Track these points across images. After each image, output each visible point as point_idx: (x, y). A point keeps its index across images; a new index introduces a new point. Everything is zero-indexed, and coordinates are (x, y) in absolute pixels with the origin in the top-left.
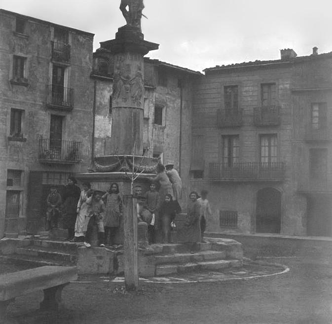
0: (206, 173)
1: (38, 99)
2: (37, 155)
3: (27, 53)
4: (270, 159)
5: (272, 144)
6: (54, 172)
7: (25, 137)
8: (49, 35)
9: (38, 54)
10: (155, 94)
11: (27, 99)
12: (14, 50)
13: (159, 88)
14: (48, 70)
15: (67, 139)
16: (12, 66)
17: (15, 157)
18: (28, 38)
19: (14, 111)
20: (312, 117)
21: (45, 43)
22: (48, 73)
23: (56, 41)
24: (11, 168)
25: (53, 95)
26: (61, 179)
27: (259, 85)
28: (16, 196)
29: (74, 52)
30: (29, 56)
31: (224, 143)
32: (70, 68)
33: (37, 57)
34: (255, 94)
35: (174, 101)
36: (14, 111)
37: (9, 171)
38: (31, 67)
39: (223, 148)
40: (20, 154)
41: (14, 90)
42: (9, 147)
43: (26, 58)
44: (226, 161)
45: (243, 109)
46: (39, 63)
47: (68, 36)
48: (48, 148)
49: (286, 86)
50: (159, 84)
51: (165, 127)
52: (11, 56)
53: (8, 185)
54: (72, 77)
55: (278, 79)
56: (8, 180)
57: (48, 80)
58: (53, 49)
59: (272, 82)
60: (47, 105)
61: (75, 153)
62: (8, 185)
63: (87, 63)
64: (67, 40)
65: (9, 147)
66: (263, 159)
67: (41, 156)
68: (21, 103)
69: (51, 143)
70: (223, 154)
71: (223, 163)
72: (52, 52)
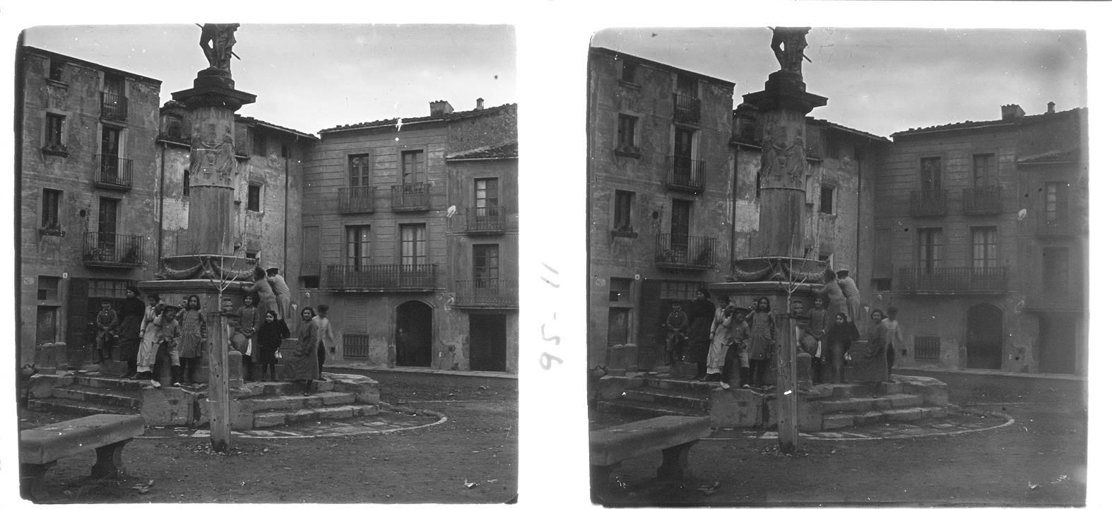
6: (105, 280)
8: (97, 84)
12: (47, 106)
16: (43, 127)
19: (47, 192)
20: (476, 199)
28: (51, 313)
31: (348, 237)
34: (393, 166)
35: (276, 178)
36: (47, 192)
39: (348, 243)
46: (83, 123)
50: (255, 153)
55: (427, 145)
56: (40, 291)
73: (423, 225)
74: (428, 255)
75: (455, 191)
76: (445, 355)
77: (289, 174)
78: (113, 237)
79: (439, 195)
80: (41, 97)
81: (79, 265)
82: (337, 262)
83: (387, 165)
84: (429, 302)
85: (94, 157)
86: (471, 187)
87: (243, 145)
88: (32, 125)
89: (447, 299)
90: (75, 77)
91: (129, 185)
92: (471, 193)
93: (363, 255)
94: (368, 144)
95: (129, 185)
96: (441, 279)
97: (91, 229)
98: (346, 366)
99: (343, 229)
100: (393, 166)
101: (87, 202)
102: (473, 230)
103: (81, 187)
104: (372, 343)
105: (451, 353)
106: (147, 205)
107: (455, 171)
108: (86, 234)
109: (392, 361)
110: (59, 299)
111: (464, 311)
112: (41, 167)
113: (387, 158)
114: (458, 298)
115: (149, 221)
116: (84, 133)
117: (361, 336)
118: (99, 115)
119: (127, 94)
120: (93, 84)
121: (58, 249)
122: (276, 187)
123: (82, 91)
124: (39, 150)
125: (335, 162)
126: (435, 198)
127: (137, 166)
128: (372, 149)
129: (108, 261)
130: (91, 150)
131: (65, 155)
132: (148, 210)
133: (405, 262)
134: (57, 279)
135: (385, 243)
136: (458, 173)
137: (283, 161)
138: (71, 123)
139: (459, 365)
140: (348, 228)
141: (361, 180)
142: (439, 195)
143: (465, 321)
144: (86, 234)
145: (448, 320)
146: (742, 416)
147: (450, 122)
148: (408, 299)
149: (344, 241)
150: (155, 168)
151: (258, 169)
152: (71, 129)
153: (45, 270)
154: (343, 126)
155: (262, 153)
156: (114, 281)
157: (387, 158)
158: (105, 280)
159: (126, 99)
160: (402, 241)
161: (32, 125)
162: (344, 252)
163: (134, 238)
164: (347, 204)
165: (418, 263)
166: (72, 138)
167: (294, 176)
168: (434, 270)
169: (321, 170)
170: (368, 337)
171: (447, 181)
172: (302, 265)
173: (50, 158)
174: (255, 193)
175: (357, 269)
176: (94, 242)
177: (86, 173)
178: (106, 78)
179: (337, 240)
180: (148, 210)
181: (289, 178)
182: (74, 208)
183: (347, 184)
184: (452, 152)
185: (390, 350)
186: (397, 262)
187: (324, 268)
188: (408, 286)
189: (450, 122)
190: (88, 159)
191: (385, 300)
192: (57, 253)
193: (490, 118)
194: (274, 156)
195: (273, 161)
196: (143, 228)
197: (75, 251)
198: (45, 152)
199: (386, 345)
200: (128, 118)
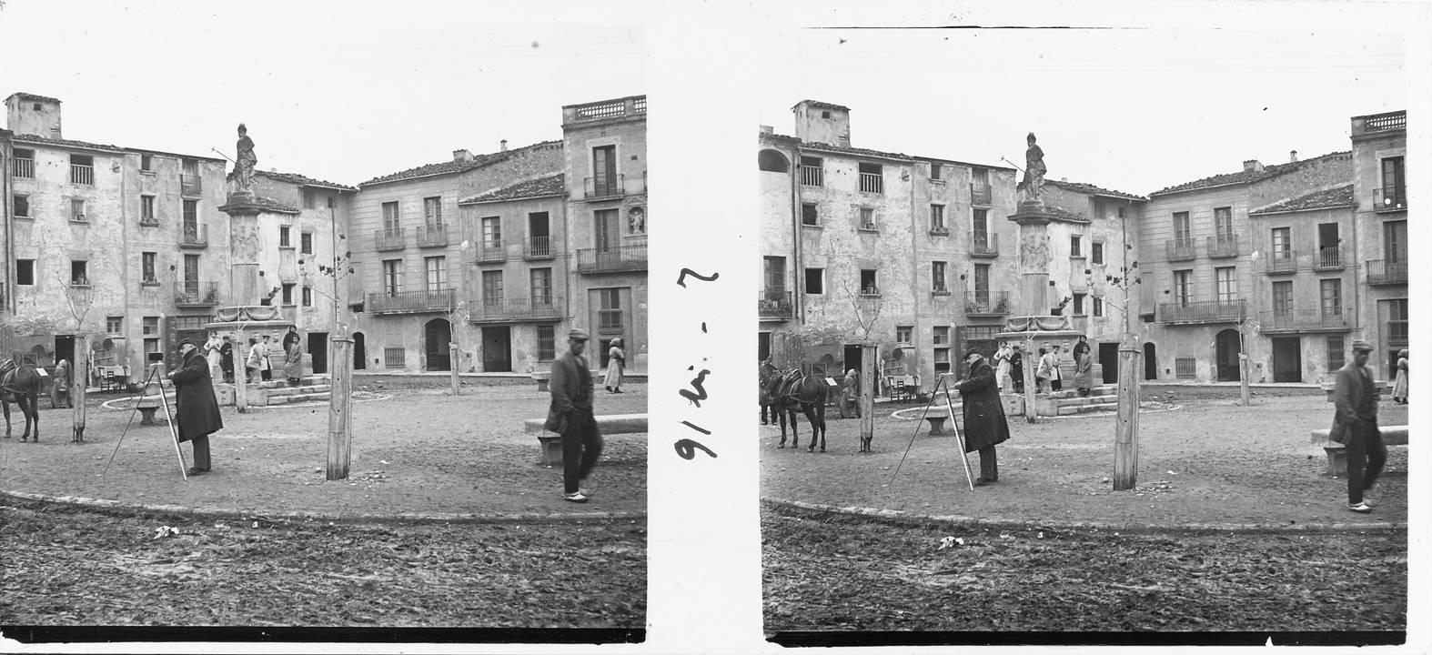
0: (366, 307)
1: (170, 238)
2: (172, 299)
3: (945, 200)
4: (1229, 297)
5: (440, 268)
6: (192, 317)
7: (949, 290)
8: (967, 178)
9: (957, 199)
10: (300, 218)
11: (158, 241)
12: (141, 190)
13: (1096, 222)
14: (178, 206)
15: (203, 280)
16: (930, 215)
17: (150, 304)
18: (154, 174)
19: (935, 263)
20: (484, 234)
21: (173, 177)
22: (178, 211)
23: (184, 173)
24: (937, 325)
25: (976, 242)
26: (199, 323)
27: (1213, 211)
28: (944, 353)
29: (205, 184)
30: (947, 203)
31: (385, 271)
32: (202, 201)
33: (167, 194)
34: (1208, 221)
35: (1115, 235)
36: (935, 263)
37: (145, 318)
38: (160, 205)
39: (1176, 284)
40: (946, 310)
41: (144, 232)
42: (933, 303)
43: (944, 206)
44: (1180, 300)
45: (1194, 239)
46: (958, 209)
47: (987, 175)
48: (974, 301)
49: (452, 199)
50: (1096, 217)
51: (1106, 266)
52: (139, 197)
53: (145, 333)
54: (994, 221)
55: (1233, 202)
56: (145, 328)
57: (970, 226)
58: (972, 191)
59: (437, 195)
60: (179, 244)
61: (213, 295)
62: (145, 333)
63: (220, 193)
64: (197, 171)
65: (933, 303)
66: (1221, 296)
67: (178, 300)
68: (152, 245)
69: (977, 295)
70: (386, 283)
71: (1177, 303)
72: (972, 195)
73: (443, 257)
74: (1238, 292)
75: (467, 229)
76: (1254, 371)
77: (1126, 231)
78: (987, 294)
79: (1245, 243)
80: (926, 193)
81: (962, 316)
82: (377, 290)
83: (1203, 220)
84: (450, 318)
85: (178, 224)
86: (1270, 235)
87: (295, 202)
88: (922, 215)
89: (1254, 326)
90: (950, 176)
91: (206, 243)
92: (480, 229)
93: (1189, 294)
94: (1188, 204)
95: (206, 243)
96: (1249, 310)
97: (179, 280)
98: (1178, 384)
99: (381, 263)
100: (1208, 221)
101: (175, 259)
102: (1272, 270)
103: (170, 248)
104: (407, 354)
105: (469, 359)
106: (1012, 266)
107: (466, 212)
108: (966, 293)
109: (423, 367)
110: (949, 342)
111: (1267, 335)
112: (930, 246)
113: (1204, 215)
114: (1263, 325)
115: (223, 270)
116: (960, 217)
117: (399, 349)
118: (180, 192)
119: (201, 174)
120: (174, 169)
121: (156, 296)
122: (1114, 243)
123: (166, 175)
124: (137, 224)
125: (1162, 219)
126: (1242, 245)
127: (211, 228)
128: (1191, 207)
129: (193, 302)
130: (966, 228)
131: (947, 235)
132: (1012, 270)
133: (431, 288)
134: (156, 318)
135: (1204, 287)
136: (1258, 224)
137: (1120, 220)
138: (950, 210)
139: (476, 369)
140: (384, 262)
141: (1184, 233)
142: (1245, 243)
143: (478, 334)
144: (966, 293)
145: (465, 332)
146: (1013, 409)
147: (1251, 183)
148: (1224, 328)
149: (382, 273)
150: (225, 229)
151: (1099, 231)
152: (950, 215)
153: (939, 323)
154: (350, 186)
155: (312, 207)
156: (199, 317)
157: (1204, 215)
158: (192, 317)
159: (200, 178)
160: (1218, 282)
161: (922, 215)
162: (383, 281)
163: (1002, 293)
164: (382, 243)
165: (441, 288)
166: (161, 213)
167: (1131, 233)
168: (452, 293)
169: (1152, 226)
170: (1194, 359)
171: (461, 221)
172: (350, 293)
173: (936, 238)
174: (307, 239)
175: (1184, 306)
176: (182, 289)
177: (173, 237)
178: (183, 161)
179: (377, 272)
180: (1012, 270)
181: (1127, 235)
182: (165, 265)
183: (382, 228)
184: (463, 197)
185: (422, 358)
186: (425, 289)
187: (1158, 307)
188: (1224, 317)
189: (1251, 183)
190: (965, 236)
191: (1207, 329)
192: (155, 299)
193: (499, 164)
194: (1113, 218)
195: (321, 212)
196: (1009, 285)
197: (169, 297)
198: (932, 234)
199: (418, 354)
200: (993, 201)
